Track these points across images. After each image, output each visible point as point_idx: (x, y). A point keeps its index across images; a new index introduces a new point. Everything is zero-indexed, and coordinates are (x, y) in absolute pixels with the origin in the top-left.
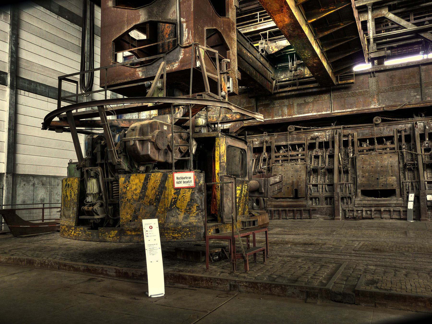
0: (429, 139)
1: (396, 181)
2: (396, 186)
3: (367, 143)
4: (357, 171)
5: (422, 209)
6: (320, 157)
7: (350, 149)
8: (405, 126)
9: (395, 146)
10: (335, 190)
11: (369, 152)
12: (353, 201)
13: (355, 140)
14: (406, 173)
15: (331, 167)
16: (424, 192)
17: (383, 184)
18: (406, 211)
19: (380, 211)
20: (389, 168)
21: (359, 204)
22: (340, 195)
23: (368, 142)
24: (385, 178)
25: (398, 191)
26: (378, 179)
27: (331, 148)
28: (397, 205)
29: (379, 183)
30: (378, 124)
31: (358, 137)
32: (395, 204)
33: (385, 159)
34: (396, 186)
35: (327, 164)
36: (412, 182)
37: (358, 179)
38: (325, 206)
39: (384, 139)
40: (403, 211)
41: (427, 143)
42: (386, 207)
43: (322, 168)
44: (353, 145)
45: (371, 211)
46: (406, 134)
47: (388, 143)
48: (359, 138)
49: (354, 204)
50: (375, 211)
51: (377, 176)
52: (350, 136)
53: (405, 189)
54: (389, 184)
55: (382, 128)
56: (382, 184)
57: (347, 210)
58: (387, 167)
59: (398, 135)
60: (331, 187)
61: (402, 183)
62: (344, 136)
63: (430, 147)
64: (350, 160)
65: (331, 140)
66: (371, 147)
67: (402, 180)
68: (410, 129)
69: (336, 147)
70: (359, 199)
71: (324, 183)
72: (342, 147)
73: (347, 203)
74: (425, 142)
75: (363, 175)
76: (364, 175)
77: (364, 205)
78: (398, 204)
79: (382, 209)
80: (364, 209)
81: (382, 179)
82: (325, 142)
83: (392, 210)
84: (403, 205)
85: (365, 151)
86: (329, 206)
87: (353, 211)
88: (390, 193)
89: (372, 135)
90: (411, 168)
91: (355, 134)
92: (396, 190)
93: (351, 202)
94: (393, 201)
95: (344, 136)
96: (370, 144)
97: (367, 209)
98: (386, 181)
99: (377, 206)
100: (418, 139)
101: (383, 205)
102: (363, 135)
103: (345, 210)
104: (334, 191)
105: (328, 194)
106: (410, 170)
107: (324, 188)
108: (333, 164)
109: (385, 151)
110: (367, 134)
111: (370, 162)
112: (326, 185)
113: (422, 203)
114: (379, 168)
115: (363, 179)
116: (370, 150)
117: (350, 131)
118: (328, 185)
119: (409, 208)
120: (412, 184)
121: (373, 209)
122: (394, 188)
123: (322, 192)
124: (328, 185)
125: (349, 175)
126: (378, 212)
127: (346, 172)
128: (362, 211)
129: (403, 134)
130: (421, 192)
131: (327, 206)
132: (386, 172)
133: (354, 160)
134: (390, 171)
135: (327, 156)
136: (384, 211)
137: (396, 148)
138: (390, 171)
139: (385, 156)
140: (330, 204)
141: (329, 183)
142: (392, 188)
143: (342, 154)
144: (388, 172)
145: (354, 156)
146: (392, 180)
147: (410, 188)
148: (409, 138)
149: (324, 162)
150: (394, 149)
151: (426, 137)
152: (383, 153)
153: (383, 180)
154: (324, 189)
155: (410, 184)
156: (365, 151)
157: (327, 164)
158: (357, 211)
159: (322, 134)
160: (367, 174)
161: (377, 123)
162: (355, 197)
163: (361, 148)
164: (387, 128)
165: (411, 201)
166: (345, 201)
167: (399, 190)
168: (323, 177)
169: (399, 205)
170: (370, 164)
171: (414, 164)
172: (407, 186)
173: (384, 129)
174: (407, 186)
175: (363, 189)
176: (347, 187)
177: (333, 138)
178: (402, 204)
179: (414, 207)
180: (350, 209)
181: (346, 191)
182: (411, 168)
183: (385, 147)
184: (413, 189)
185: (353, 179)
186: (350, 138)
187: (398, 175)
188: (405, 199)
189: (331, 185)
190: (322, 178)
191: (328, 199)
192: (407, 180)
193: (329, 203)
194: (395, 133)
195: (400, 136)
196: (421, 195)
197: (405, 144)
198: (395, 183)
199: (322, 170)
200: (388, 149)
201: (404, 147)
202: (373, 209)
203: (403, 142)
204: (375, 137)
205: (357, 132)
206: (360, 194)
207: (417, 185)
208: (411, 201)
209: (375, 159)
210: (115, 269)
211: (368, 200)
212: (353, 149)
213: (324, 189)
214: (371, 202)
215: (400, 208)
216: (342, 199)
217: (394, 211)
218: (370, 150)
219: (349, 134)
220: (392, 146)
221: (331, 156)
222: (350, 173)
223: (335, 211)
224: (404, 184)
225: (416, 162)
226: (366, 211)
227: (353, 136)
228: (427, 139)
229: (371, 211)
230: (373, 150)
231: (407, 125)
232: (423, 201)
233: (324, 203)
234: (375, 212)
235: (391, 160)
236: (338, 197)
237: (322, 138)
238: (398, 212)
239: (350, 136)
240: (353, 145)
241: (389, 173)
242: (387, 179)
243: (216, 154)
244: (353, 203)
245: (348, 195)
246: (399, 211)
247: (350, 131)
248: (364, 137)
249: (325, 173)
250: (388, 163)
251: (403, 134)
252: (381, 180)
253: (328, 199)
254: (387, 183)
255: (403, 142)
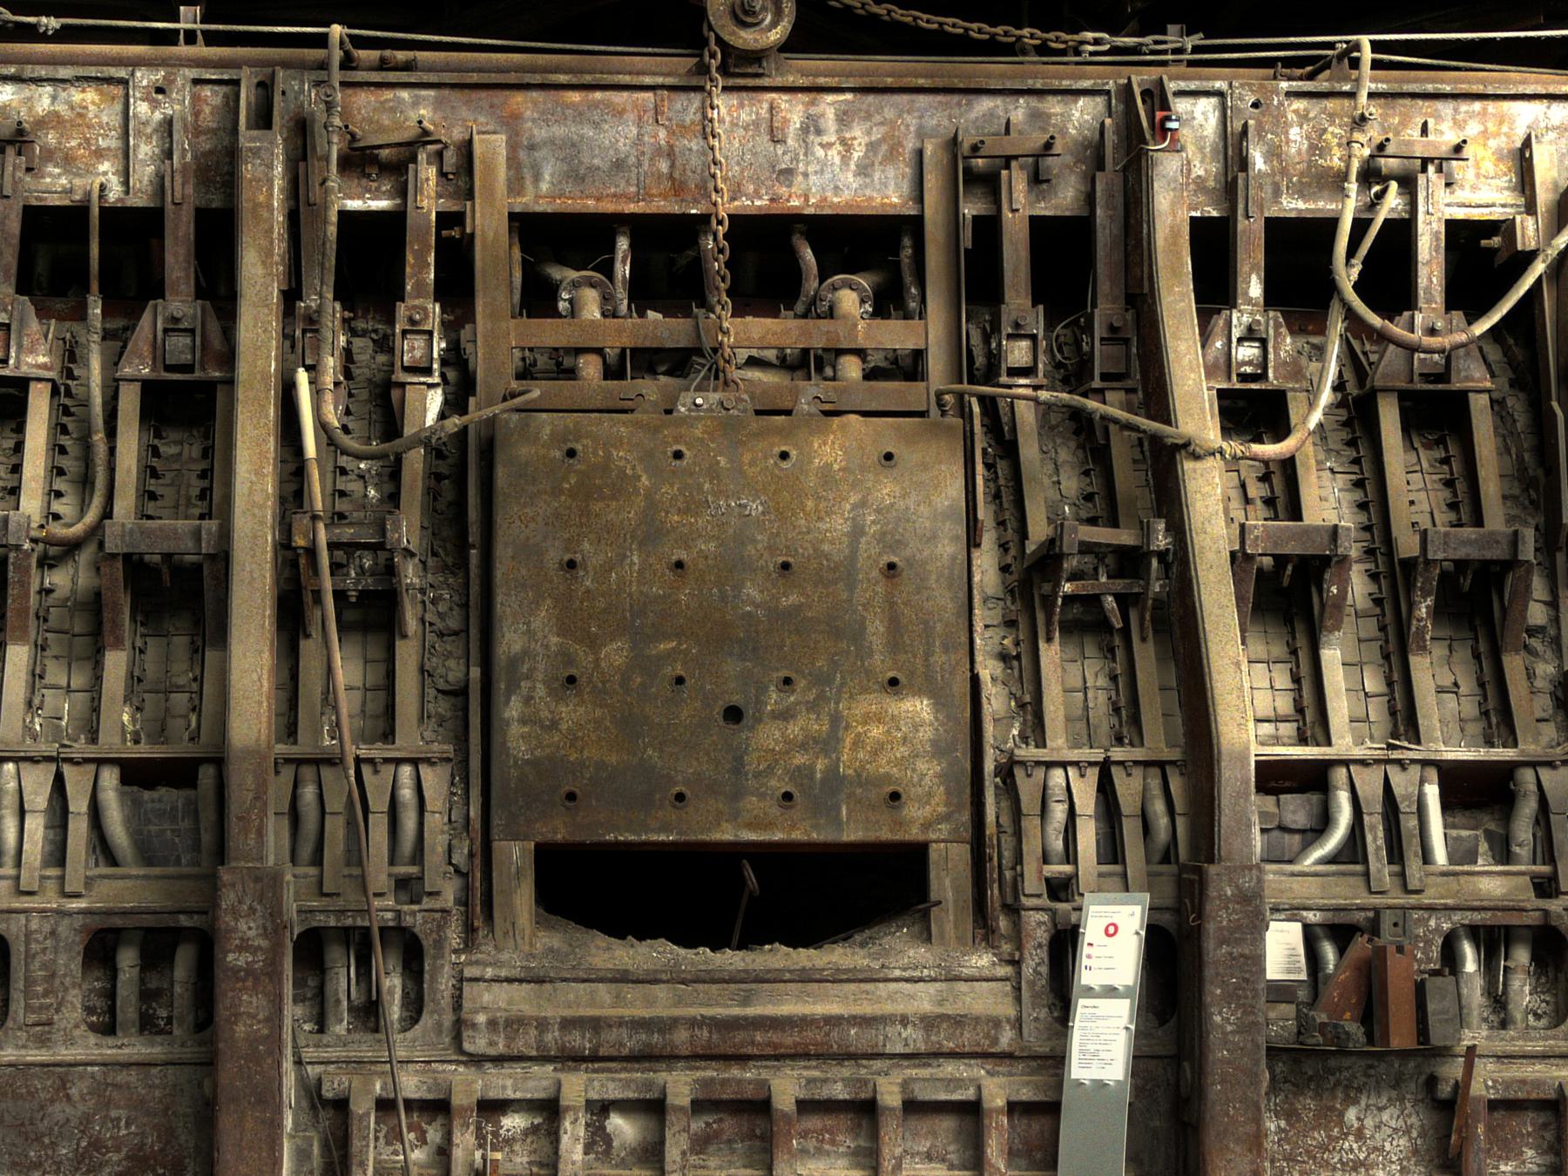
0: (1273, 298)
1: (939, 749)
2: (928, 815)
3: (607, 269)
4: (506, 603)
5: (1215, 1089)
6: (39, 408)
7: (414, 328)
8: (1036, 116)
9: (930, 330)
10: (239, 840)
11: (652, 388)
12: (445, 984)
13: (488, 224)
14: (1051, 654)
15: (177, 532)
16: (1247, 882)
17: (804, 773)
18: (1051, 1109)
19: (760, 1106)
20: (870, 588)
21: (514, 1024)
22: (291, 907)
23: (623, 270)
24: (813, 707)
25: (948, 876)
26: (734, 714)
27: (180, 302)
28: (947, 1039)
29: (753, 763)
30: (755, 57)
31: (516, 186)
32: (929, 1023)
33: (826, 475)
34: (938, 805)
35: (125, 505)
36: (1105, 768)
37: (512, 710)
38: (86, 1048)
39: (808, 255)
40: (1014, 1108)
41: (1250, 335)
42: (824, 1056)
43: (58, 553)
44: (456, 285)
45: (653, 1108)
46: (1043, 209)
47: (848, 301)
48: (528, 202)
49: (460, 1026)
50: (698, 1106)
51: (729, 677)
52: (428, 173)
53: (1031, 848)
54: (864, 780)
55: (793, 111)
56: (778, 785)
57: (362, 1106)
58: (846, 572)
59: (969, 210)
60: (165, 796)
61: (1007, 772)
62: (360, 161)
63: (1273, 380)
64: (415, 461)
65: (184, 192)
66: (658, 327)
67: (1001, 731)
68: (1093, 154)
69: (259, 271)
70: (512, 960)
71: (81, 748)
72: (320, 296)
73: (369, 1013)
74: (1240, 319)
75: (567, 658)
76: (584, 657)
77: (581, 1041)
78: (958, 1021)
79: (786, 1087)
80: (576, 1087)
81: (785, 715)
82: (115, 217)
83: (890, 1095)
84: (1006, 1039)
85: (590, 368)
86: (133, 1047)
87: (438, 1107)
88: (858, 889)
89: (677, 188)
90: (1094, 600)
91: (492, 147)
92: (935, 852)
93: (415, 1006)
94: (908, 986)
95: (360, 161)
96: (643, 294)
97: (610, 1086)
98: (828, 744)
99: (725, 1045)
100: (1176, 273)
101: (789, 1039)
102: (576, 175)
103: (341, 1105)
104: (221, 853)
105: (127, 891)
106: (1086, 623)
107: (79, 805)
108: (213, 496)
109: (808, 393)
110: (619, 165)
111: (652, 504)
112: (110, 777)
113: (1221, 1018)
114: (751, 591)
115: (570, 713)
116: (646, 360)
117: (417, 110)
118: (135, 774)
119: (1080, 1069)
120: (1106, 789)
121: (680, 1085)
122: (914, 834)
123: (58, 854)
124: (135, 774)
125: (407, 655)
126: (729, 1125)
127: (374, 615)
128: (550, 1110)
129: (1021, 205)
130: (1221, 885)
131: (108, 1049)
132: (837, 633)
133: (464, 477)
134: (876, 629)
135: (129, 401)
136: (805, 1106)
137: (937, 365)
138: (876, 629)
139: (831, 449)
140: (147, 1025)
141: (144, 751)
142: (885, 835)
143: (328, 380)
144: (858, 634)
145: (478, 411)
146: (900, 734)
147: (1088, 837)
148: (1082, 270)
149: (80, 467)
150: (909, 367)
151: (1243, 266)
152: (804, 405)
153: (794, 730)
154: (79, 828)
155: (1085, 794)
156: (590, 368)
157: (125, 505)
158: (492, 1108)
159: (80, 112)
160: (615, 653)
161: (747, 38)
162: (469, 930)
163: (548, 333)
164: (844, 119)
165: (1110, 992)
166: (342, 980)
167: (961, 854)
168: (70, 660)
169: (967, 1039)
170: (650, 533)
171: (1129, 561)
172: (1059, 812)
173: (812, 126)
174: (1059, 812)
175: (559, 831)
176: (379, 803)
177: (220, 169)
178: (996, 1023)
179: (1140, 1060)
180: (411, 1085)
181: (355, 854)
182: (1094, 600)
183: (816, 335)
184: (1112, 850)
185: (443, 707)
186: (429, 196)
187: (961, 686)
188: (1035, 962)
189: (179, 776)
190: (56, 674)
191: (127, 959)
192: (1058, 744)
193: (128, 1009)
194: (932, 182)
195: (988, 228)
196: (1219, 918)
197: (1036, 322)
198: (929, 769)
199: (59, 579)
200: (851, 368)
201: (1018, 353)
202: (680, 1085)
203: (1017, 299)
204: (726, 207)
205: (511, 124)
206: (521, 899)
207: (1159, 807)
208: (1110, 992)
209: (714, 473)
210: (1104, 403)
211: (622, 978)
212: (451, 328)
213: (79, 828)
214: (661, 1003)
215: (978, 1071)
216: (311, 950)
217: (914, 1107)
218: (646, 360)
219: (425, 137)
220: (895, 336)
221: (188, 407)
222: (412, 624)
223: (226, 1121)
224: (1027, 788)
225: (1161, 540)
226: (601, 1109)
227: (462, 170)
228: (1255, 289)
229: (653, 1108)
230: (678, 362)
231: (1054, 106)
232: (1231, 997)
233: (72, 1014)
234: (697, 1125)
235: (886, 490)
236: (274, 927)
237: (68, 161)
238: (947, 1124)
239: (428, 173)
240: (456, 285)
241: (864, 652)
242: (836, 719)
243: (1381, 834)
244: (437, 1016)
245: (385, 908)
246: (971, 1110)
247: (417, 110)
248: (591, 205)
249: (94, 606)
250: (857, 532)
251: (1021, 205)
252: (769, 736)
253: (127, 959)
254: (832, 773)
255: (1017, 299)
